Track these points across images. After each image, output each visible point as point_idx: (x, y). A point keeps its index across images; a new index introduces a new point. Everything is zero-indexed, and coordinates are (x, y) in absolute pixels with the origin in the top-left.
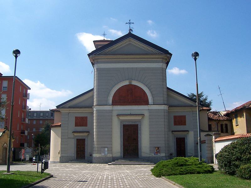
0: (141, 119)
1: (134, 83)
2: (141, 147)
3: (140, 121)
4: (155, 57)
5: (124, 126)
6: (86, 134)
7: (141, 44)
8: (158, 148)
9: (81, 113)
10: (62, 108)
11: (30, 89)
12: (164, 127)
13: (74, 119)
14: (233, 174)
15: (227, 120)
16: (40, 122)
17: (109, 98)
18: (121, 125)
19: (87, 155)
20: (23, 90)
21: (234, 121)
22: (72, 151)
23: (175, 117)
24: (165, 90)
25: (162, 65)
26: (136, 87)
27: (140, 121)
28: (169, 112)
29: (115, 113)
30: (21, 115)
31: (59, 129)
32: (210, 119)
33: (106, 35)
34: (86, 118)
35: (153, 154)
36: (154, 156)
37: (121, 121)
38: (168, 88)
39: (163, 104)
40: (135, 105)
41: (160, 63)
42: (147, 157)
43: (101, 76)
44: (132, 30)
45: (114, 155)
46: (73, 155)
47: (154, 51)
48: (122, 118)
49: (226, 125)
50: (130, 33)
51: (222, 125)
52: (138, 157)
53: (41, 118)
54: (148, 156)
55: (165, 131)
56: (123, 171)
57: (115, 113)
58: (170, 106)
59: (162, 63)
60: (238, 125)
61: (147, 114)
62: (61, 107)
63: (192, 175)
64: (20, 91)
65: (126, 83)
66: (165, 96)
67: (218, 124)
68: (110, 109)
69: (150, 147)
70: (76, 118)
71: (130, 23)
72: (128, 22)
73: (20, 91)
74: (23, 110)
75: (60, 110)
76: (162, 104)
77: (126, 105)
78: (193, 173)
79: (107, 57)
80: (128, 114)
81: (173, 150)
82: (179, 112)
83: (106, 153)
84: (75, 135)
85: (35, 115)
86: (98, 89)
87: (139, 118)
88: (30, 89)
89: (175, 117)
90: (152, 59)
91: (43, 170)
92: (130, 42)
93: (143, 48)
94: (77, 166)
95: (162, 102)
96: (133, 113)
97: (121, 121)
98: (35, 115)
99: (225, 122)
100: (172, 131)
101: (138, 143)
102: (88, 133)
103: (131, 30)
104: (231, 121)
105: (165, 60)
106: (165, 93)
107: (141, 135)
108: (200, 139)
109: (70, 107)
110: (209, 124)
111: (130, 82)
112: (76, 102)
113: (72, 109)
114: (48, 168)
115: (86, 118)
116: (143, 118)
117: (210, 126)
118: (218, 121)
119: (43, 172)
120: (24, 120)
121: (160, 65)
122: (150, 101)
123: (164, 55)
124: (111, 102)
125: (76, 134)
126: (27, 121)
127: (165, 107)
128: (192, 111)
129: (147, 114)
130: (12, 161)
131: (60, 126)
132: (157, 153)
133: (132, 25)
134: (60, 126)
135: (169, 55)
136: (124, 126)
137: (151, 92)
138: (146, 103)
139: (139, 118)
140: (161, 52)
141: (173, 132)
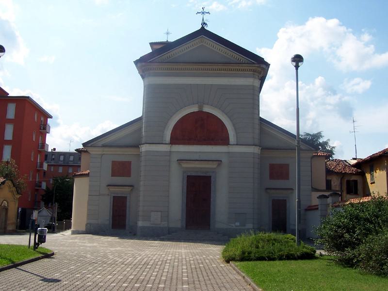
0: (215, 168)
1: (207, 109)
6: (128, 189)
7: (217, 46)
9: (123, 155)
10: (91, 146)
11: (51, 117)
13: (110, 165)
14: (348, 263)
15: (357, 174)
19: (129, 221)
20: (39, 118)
21: (368, 176)
22: (105, 216)
23: (272, 167)
24: (257, 122)
26: (209, 115)
29: (175, 158)
30: (36, 159)
31: (85, 180)
32: (329, 172)
33: (165, 32)
34: (129, 163)
38: (262, 120)
43: (152, 96)
44: (206, 24)
45: (172, 225)
46: (107, 223)
47: (240, 58)
48: (185, 165)
49: (356, 182)
50: (203, 28)
51: (348, 182)
52: (209, 228)
53: (71, 163)
56: (208, 248)
60: (374, 183)
61: (225, 160)
62: (89, 145)
63: (272, 262)
64: (36, 119)
65: (194, 109)
66: (257, 131)
68: (167, 150)
70: (114, 163)
73: (36, 119)
74: (39, 149)
75: (89, 149)
77: (193, 144)
78: (274, 259)
80: (195, 159)
81: (267, 217)
82: (279, 159)
83: (156, 219)
84: (111, 189)
85: (62, 158)
87: (213, 165)
88: (51, 117)
89: (272, 167)
90: (232, 71)
91: (36, 245)
94: (109, 240)
98: (62, 158)
99: (353, 178)
100: (267, 189)
102: (132, 187)
103: (204, 23)
104: (363, 175)
105: (258, 74)
106: (257, 127)
108: (299, 202)
109: (104, 146)
110: (327, 179)
111: (201, 107)
112: (107, 141)
113: (106, 149)
114: (44, 242)
115: (129, 163)
116: (219, 165)
117: (328, 184)
118: (342, 175)
119: (37, 248)
120: (41, 165)
121: (252, 81)
122: (232, 139)
123: (256, 65)
124: (168, 138)
125: (112, 189)
126: (45, 167)
130: (17, 228)
131: (87, 175)
133: (206, 17)
134: (87, 175)
135: (264, 66)
137: (234, 125)
138: (225, 141)
139: (213, 165)
140: (247, 57)
141: (269, 191)
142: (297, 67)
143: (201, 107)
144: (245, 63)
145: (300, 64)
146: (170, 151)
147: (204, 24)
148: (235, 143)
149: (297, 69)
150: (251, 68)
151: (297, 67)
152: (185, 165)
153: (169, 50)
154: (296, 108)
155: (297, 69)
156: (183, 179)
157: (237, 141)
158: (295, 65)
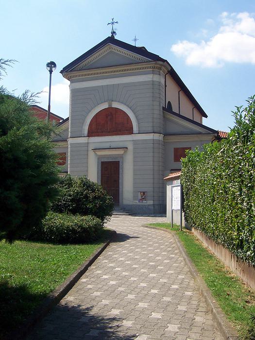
0: (123, 154)
1: (115, 105)
2: (122, 191)
3: (122, 156)
4: (135, 67)
5: (102, 163)
8: (144, 193)
11: (206, 116)
12: (152, 164)
16: (216, 136)
17: (84, 127)
18: (98, 162)
25: (153, 77)
27: (122, 156)
28: (165, 143)
29: (91, 147)
35: (137, 202)
36: (139, 204)
37: (99, 157)
39: (152, 131)
40: (98, 136)
41: (149, 75)
42: (129, 205)
48: (100, 153)
54: (131, 203)
55: (153, 170)
57: (91, 147)
58: (165, 135)
59: (152, 75)
61: (130, 147)
65: (105, 106)
67: (137, 335)
69: (134, 192)
71: (113, 23)
72: (111, 21)
76: (151, 132)
79: (81, 74)
86: (71, 118)
87: (121, 152)
92: (110, 50)
93: (124, 55)
95: (150, 129)
96: (113, 145)
97: (99, 157)
101: (118, 187)
107: (123, 176)
111: (110, 105)
116: (125, 152)
122: (135, 128)
123: (153, 63)
124: (86, 132)
127: (158, 137)
128: (201, 141)
129: (130, 147)
132: (142, 199)
133: (115, 26)
136: (102, 163)
137: (136, 117)
138: (130, 131)
139: (121, 152)
142: (51, 72)
143: (110, 105)
144: (145, 62)
145: (53, 69)
146: (88, 143)
147: (113, 33)
148: (138, 132)
149: (51, 73)
150: (150, 66)
151: (51, 72)
152: (100, 153)
153: (81, 61)
154: (48, 105)
155: (51, 73)
156: (98, 165)
157: (139, 131)
158: (49, 69)
